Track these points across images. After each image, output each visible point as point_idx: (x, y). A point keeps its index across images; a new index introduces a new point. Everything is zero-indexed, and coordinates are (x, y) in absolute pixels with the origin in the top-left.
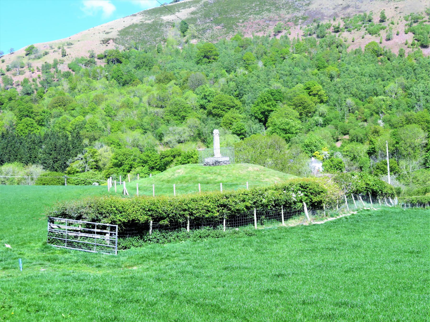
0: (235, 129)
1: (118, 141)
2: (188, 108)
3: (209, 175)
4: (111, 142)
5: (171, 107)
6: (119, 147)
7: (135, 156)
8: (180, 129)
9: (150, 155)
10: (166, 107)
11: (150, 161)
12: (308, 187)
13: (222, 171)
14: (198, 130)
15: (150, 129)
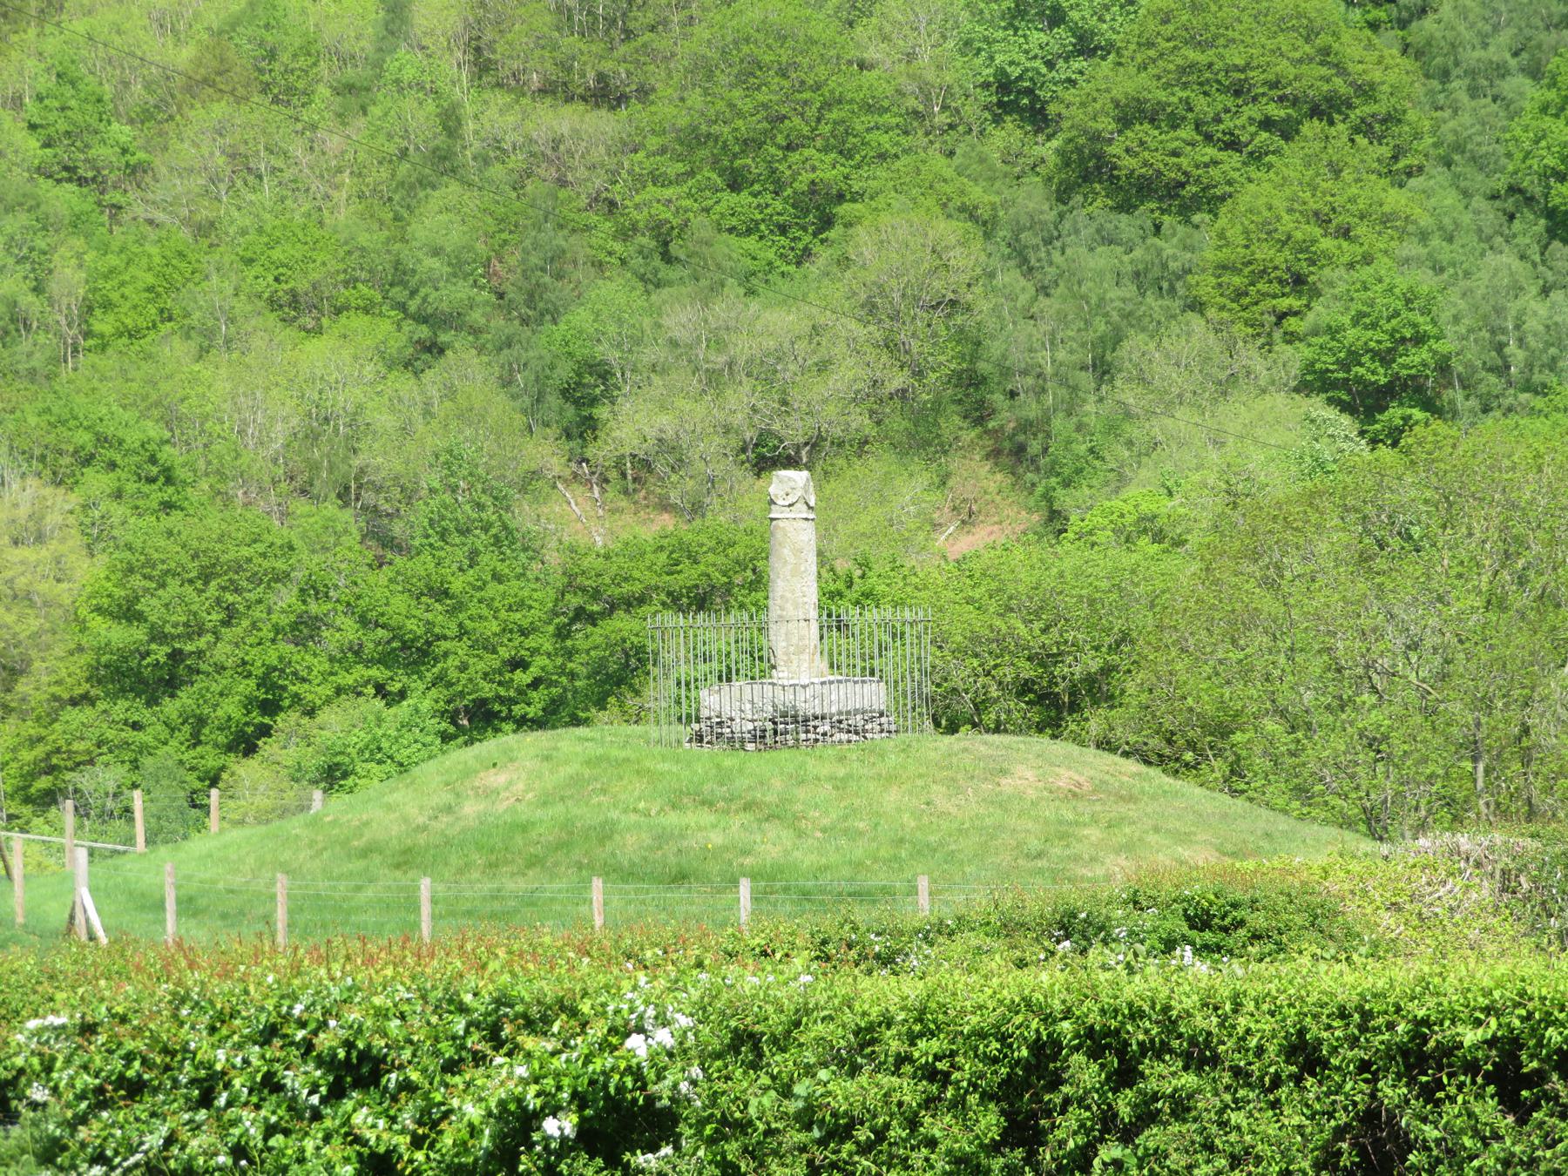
0: (1333, 331)
1: (154, 431)
2: (869, 109)
3: (706, 817)
4: (84, 438)
5: (695, 98)
6: (157, 494)
7: (313, 590)
8: (772, 322)
9: (457, 585)
10: (644, 93)
11: (461, 648)
12: (1241, 923)
13: (801, 793)
14: (961, 335)
15: (476, 317)
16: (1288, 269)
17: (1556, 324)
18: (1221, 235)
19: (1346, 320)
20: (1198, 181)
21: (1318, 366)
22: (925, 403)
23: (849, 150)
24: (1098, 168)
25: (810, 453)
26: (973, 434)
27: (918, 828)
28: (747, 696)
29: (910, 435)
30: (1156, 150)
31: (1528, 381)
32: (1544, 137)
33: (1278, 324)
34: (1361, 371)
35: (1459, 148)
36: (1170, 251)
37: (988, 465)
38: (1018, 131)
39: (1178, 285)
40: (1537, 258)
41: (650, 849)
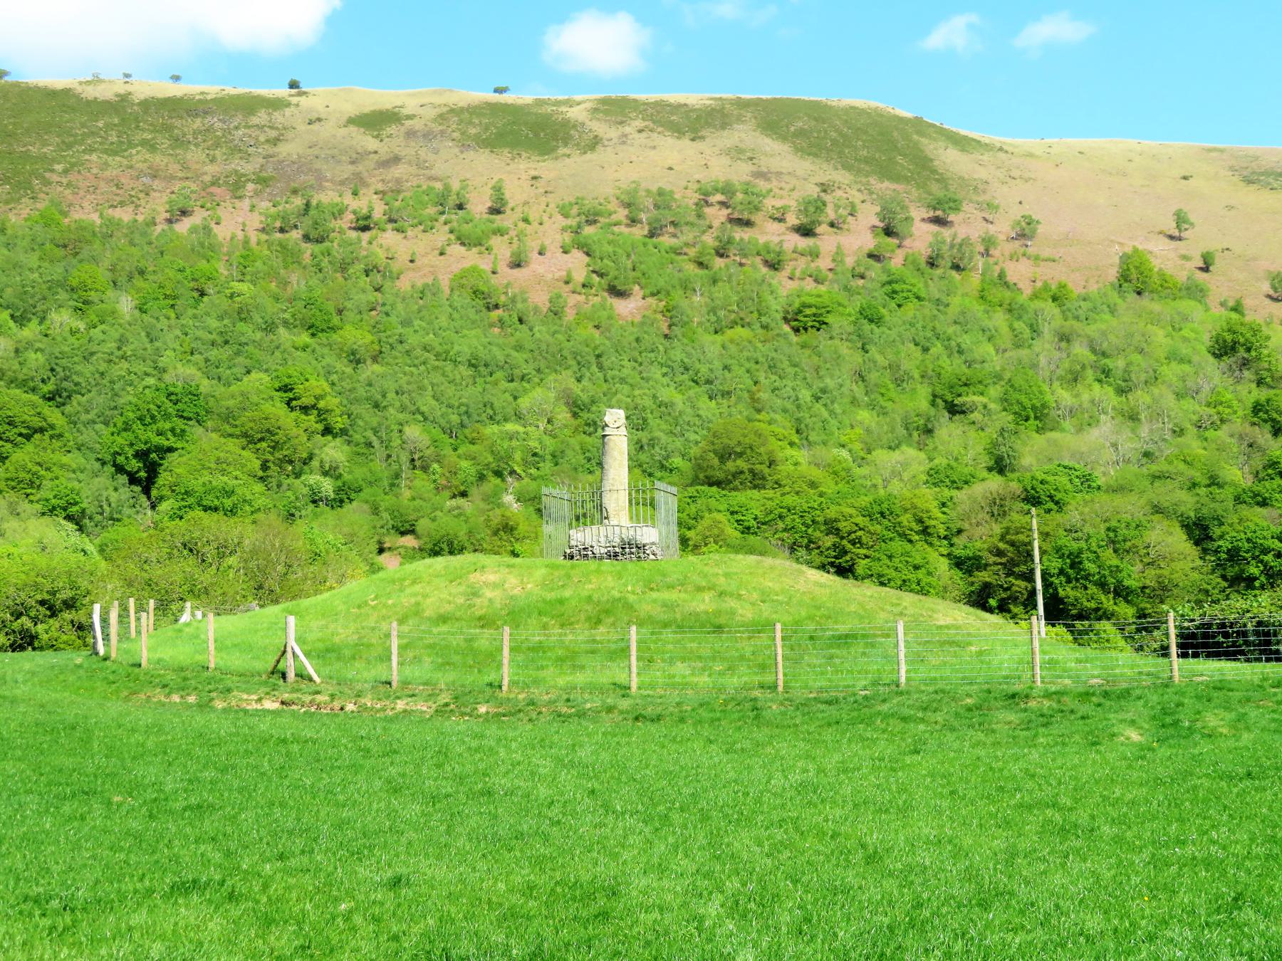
0: (47, 500)
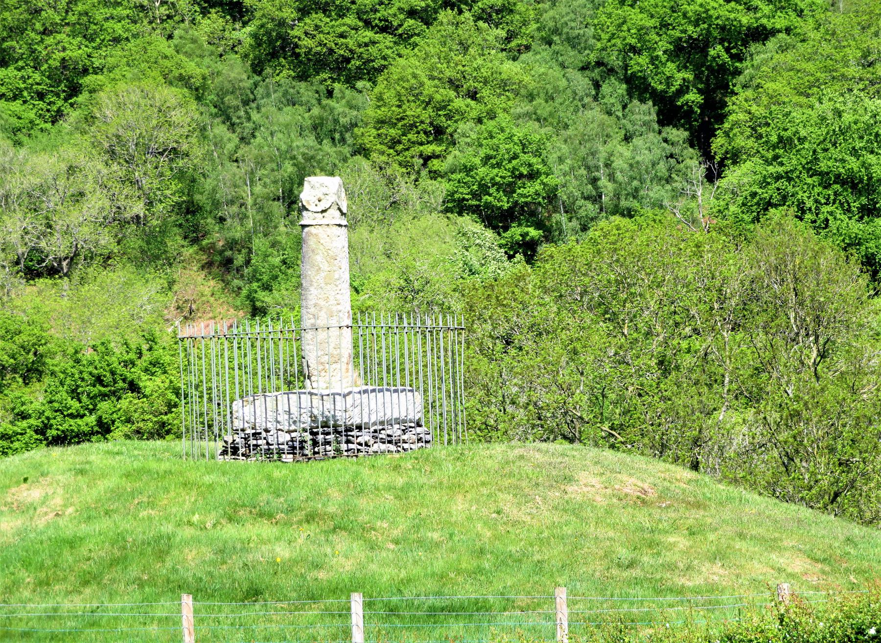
0: (468, 170)
3: (265, 529)
13: (362, 503)
14: (181, 175)
16: (431, 124)
17: (638, 162)
18: (380, 98)
19: (477, 161)
20: (360, 57)
21: (456, 196)
22: (155, 227)
23: (91, 35)
24: (283, 48)
25: (70, 265)
26: (191, 251)
27: (496, 537)
28: (283, 405)
29: (143, 252)
30: (328, 33)
31: (616, 206)
32: (624, 22)
33: (425, 165)
34: (490, 199)
35: (556, 31)
36: (341, 110)
37: (203, 274)
38: (221, 20)
39: (347, 135)
40: (620, 114)
41: (213, 563)
